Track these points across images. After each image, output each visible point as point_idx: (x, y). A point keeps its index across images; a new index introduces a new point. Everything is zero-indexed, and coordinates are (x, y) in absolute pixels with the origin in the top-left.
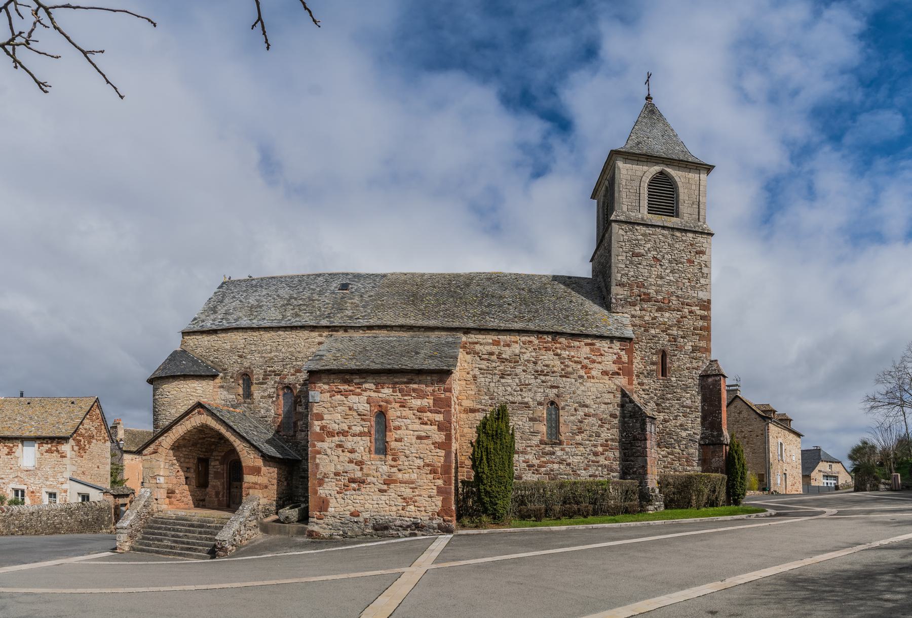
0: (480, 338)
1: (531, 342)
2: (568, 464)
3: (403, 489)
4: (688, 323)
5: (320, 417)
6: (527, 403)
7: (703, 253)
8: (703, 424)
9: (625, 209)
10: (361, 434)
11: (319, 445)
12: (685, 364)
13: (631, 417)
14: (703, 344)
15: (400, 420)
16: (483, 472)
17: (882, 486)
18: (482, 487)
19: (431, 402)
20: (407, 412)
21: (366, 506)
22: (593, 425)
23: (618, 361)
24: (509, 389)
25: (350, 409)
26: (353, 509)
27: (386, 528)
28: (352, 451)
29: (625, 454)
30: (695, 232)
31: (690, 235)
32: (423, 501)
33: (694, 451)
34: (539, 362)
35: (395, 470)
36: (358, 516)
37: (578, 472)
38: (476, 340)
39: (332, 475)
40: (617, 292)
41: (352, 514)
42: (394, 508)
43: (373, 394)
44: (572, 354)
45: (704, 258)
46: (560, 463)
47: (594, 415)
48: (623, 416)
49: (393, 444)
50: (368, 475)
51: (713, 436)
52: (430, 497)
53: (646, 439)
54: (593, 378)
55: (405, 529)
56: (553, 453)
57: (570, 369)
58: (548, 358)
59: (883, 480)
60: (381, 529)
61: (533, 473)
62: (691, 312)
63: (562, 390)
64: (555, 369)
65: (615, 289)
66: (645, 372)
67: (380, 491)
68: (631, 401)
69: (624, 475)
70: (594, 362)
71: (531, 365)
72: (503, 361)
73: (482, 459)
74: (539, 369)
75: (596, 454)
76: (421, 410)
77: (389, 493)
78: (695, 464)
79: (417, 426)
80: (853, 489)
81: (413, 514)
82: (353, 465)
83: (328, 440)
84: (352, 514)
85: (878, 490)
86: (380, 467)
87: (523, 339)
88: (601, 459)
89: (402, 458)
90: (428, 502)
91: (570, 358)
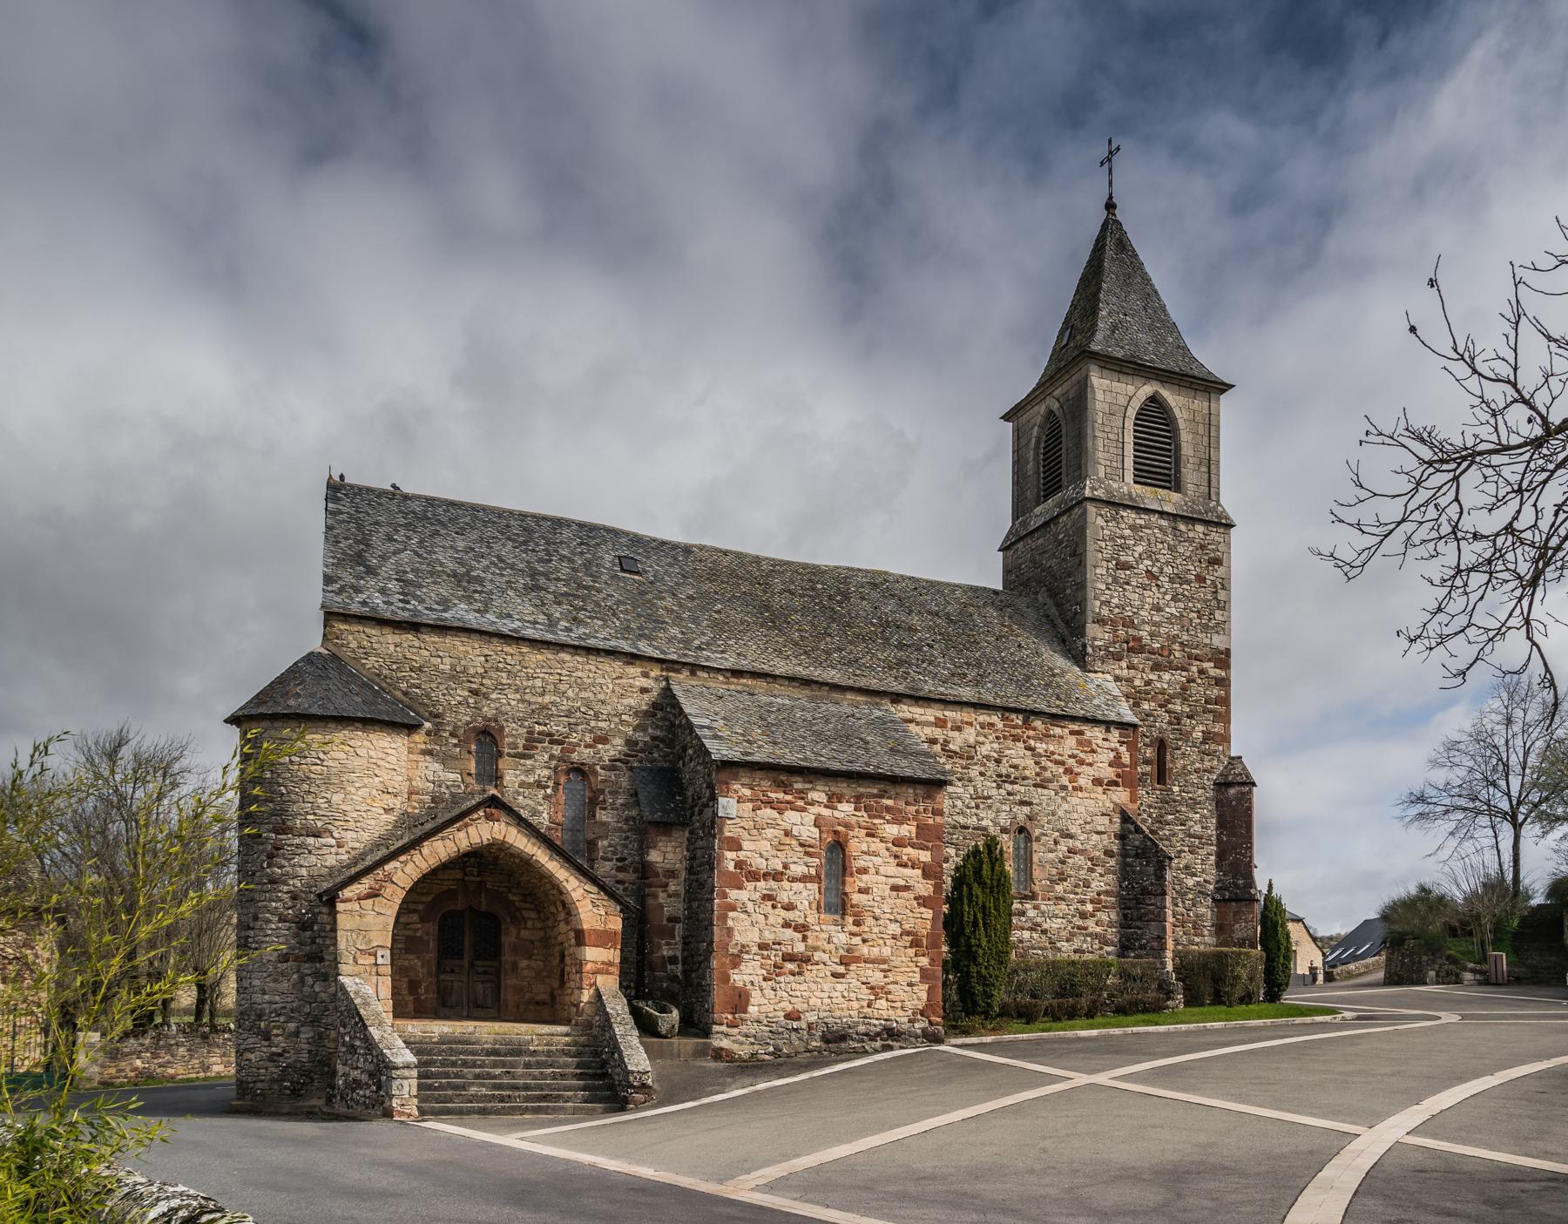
0: (917, 712)
1: (992, 725)
2: (1044, 932)
3: (870, 972)
4: (1198, 691)
5: (735, 845)
8: (1218, 865)
9: (1102, 475)
10: (804, 879)
11: (734, 894)
13: (1137, 856)
15: (866, 857)
16: (979, 945)
17: (1468, 976)
18: (973, 969)
19: (914, 829)
20: (876, 845)
21: (812, 1002)
22: (1080, 868)
23: (1116, 762)
24: (959, 803)
25: (787, 833)
26: (789, 1008)
27: (843, 1038)
28: (789, 907)
29: (1125, 916)
31: (1200, 528)
32: (899, 992)
33: (1205, 910)
35: (857, 940)
36: (799, 1019)
38: (909, 716)
39: (755, 949)
40: (1097, 635)
41: (788, 1016)
42: (855, 1005)
43: (826, 812)
45: (1221, 571)
46: (1031, 929)
47: (1082, 852)
48: (1124, 854)
49: (856, 898)
50: (816, 949)
51: (1237, 886)
52: (910, 985)
53: (1164, 894)
54: (1081, 789)
55: (873, 1039)
57: (1048, 774)
58: (1016, 752)
59: (1471, 965)
60: (837, 1041)
62: (1201, 672)
64: (1027, 773)
65: (1092, 630)
67: (834, 975)
68: (1138, 830)
69: (1124, 948)
70: (1081, 762)
71: (992, 765)
72: (951, 755)
73: (975, 924)
74: (1004, 772)
75: (1083, 915)
76: (899, 842)
79: (892, 869)
80: (1380, 975)
81: (885, 1014)
83: (750, 886)
84: (788, 1016)
85: (1458, 981)
86: (834, 935)
87: (982, 718)
88: (1090, 924)
89: (870, 921)
90: (907, 991)
91: (1049, 755)
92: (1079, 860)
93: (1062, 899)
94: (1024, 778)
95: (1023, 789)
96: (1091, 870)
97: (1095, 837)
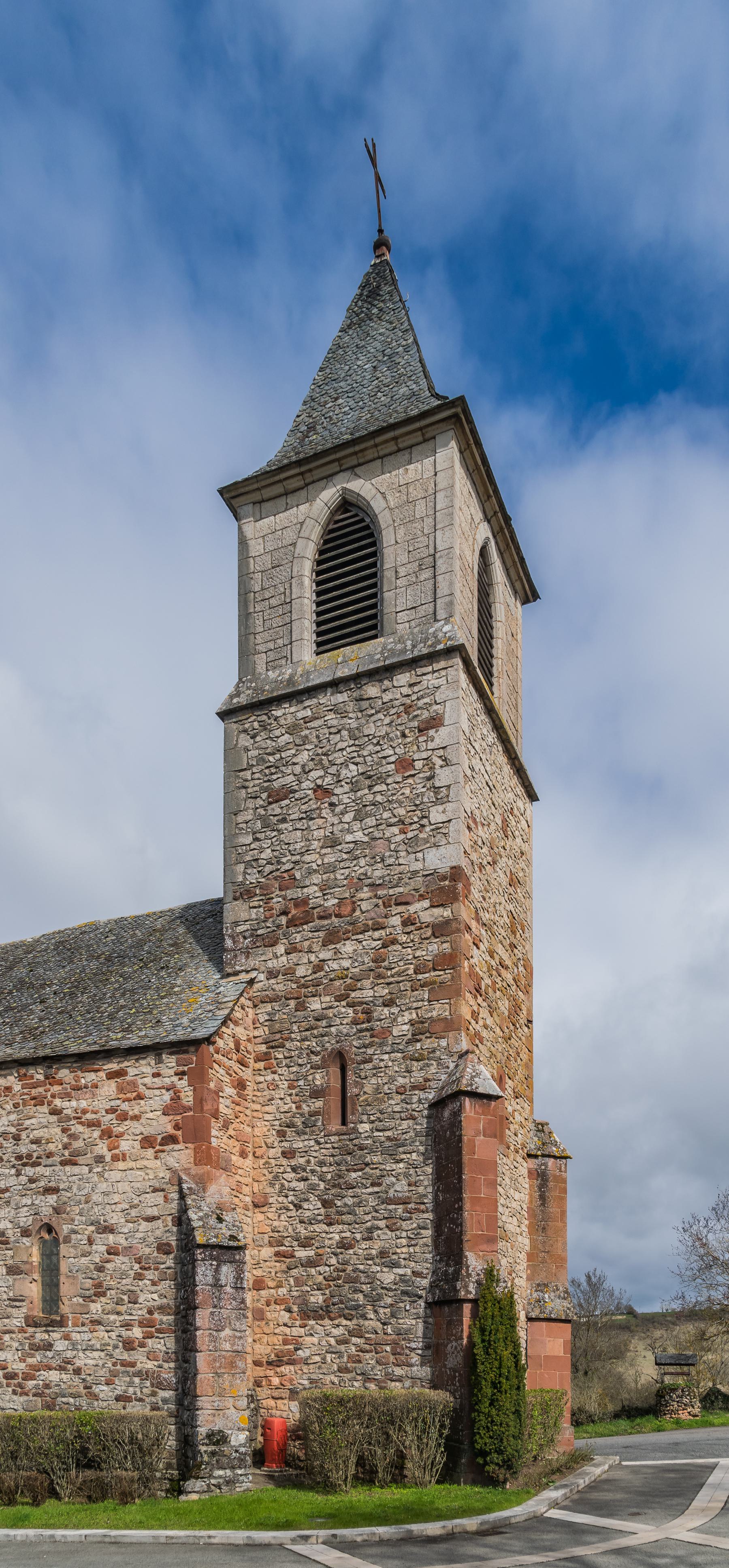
2: (77, 1371)
7: (435, 722)
12: (392, 1080)
22: (123, 1275)
30: (413, 663)
31: (403, 679)
34: (24, 1135)
37: (96, 1389)
44: (84, 1104)
46: (61, 1369)
56: (49, 1346)
57: (78, 1144)
61: (14, 1392)
64: (51, 1147)
66: (298, 1121)
70: (123, 1117)
75: (129, 1345)
78: (415, 1359)
88: (139, 1357)
92: (120, 1262)
93: (99, 1322)
94: (49, 1155)
95: (47, 1171)
96: (139, 1277)
97: (144, 1226)
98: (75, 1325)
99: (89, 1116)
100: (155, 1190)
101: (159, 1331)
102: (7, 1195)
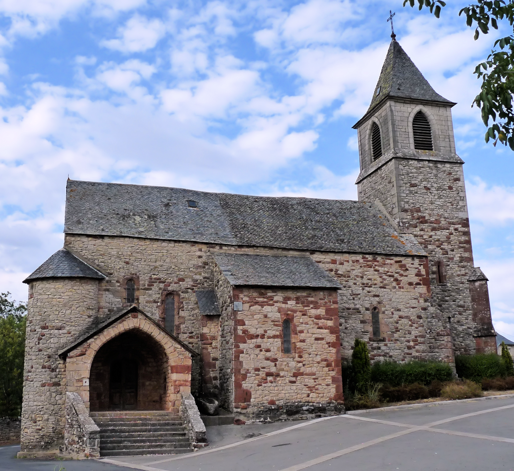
6: (358, 309)
7: (458, 179)
10: (275, 337)
14: (466, 255)
19: (324, 311)
20: (305, 319)
23: (418, 275)
24: (345, 298)
28: (268, 350)
31: (448, 165)
35: (301, 364)
43: (283, 306)
45: (460, 183)
46: (384, 356)
56: (379, 348)
57: (385, 282)
58: (370, 273)
62: (456, 229)
63: (382, 298)
70: (402, 275)
75: (409, 348)
76: (318, 317)
77: (298, 383)
82: (268, 362)
89: (306, 356)
92: (404, 321)
93: (398, 340)
94: (376, 284)
95: (374, 289)
98: (389, 341)
99: (389, 274)
100: (415, 299)
101: (419, 343)
102: (359, 296)
